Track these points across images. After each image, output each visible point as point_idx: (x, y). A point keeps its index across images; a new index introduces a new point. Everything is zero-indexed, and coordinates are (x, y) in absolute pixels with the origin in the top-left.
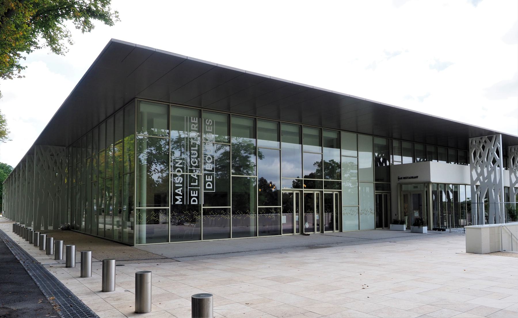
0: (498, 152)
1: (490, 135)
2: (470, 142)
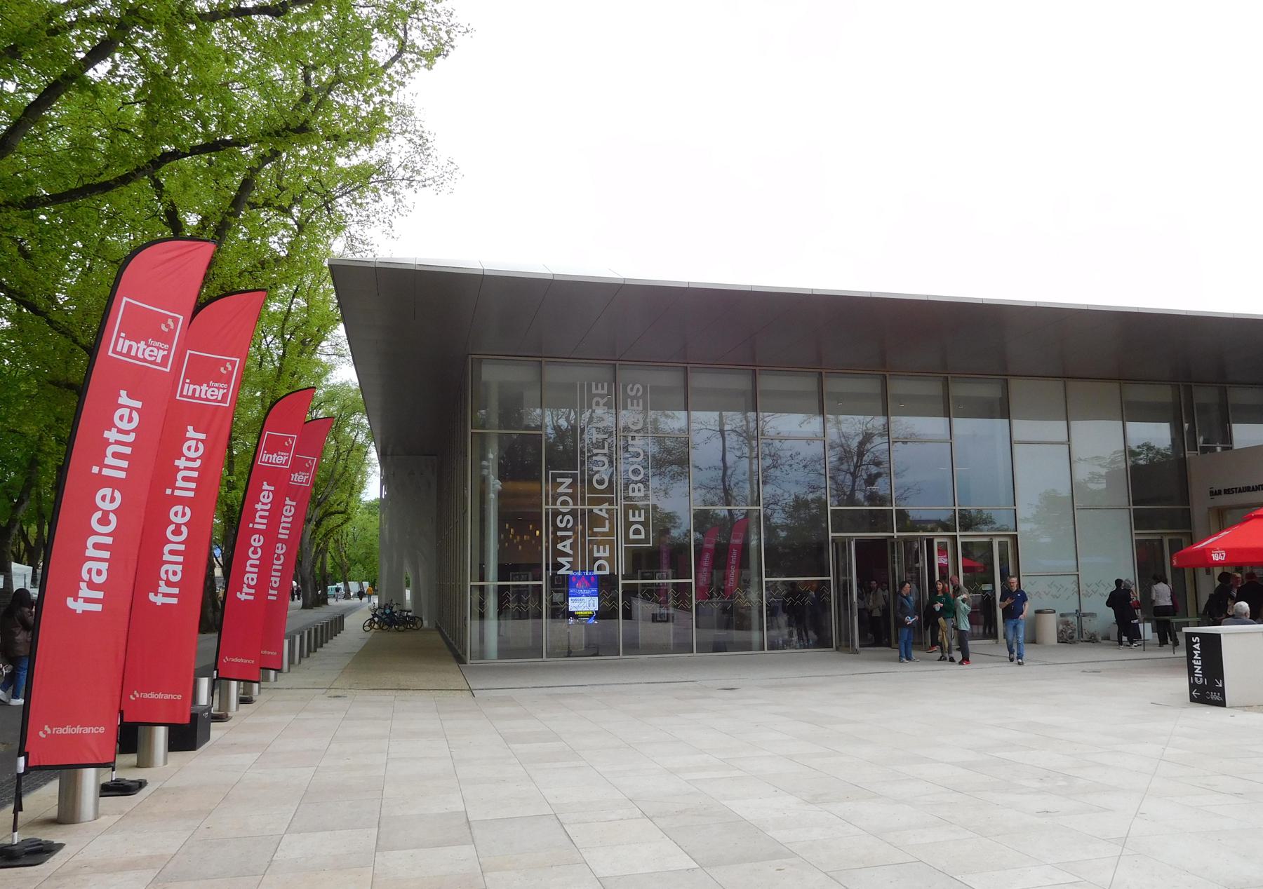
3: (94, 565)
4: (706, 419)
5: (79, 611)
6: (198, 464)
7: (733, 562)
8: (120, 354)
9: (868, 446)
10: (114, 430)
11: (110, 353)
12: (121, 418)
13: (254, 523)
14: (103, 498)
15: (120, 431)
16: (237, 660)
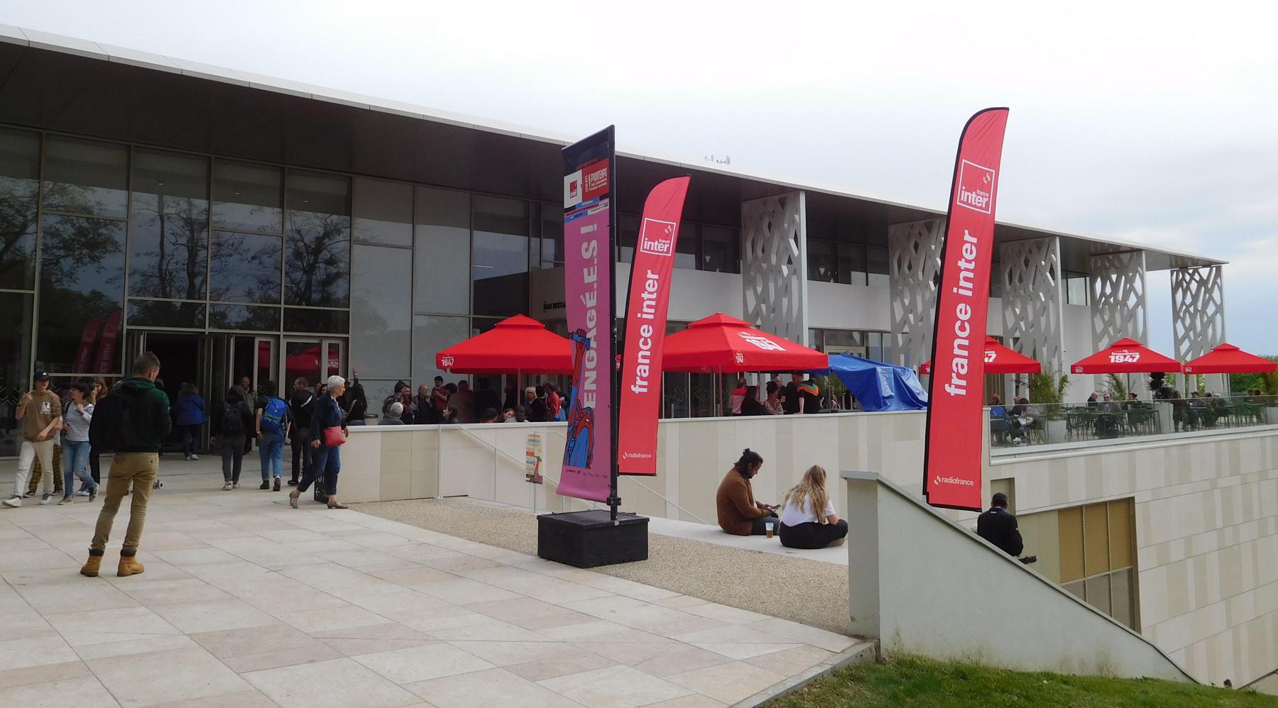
0: (1052, 272)
4: (146, 203)
6: (654, 296)
7: (83, 360)
9: (326, 241)
13: (642, 313)
16: (635, 455)
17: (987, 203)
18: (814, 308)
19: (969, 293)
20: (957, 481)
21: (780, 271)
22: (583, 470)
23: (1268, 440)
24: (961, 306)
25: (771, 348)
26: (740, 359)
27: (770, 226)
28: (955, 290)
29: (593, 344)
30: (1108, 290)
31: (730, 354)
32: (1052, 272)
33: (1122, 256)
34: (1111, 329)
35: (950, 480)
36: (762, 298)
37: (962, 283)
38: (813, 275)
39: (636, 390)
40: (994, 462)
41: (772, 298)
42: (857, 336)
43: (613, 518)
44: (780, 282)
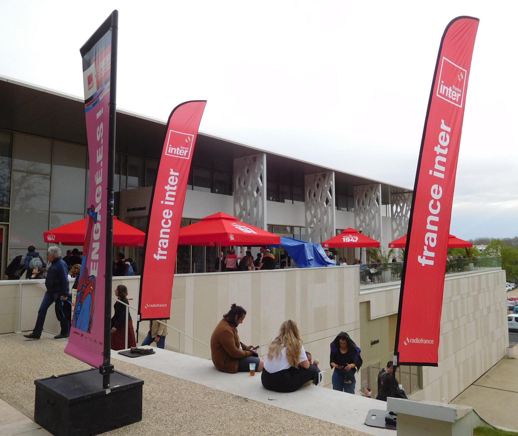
0: (378, 201)
1: (322, 173)
2: (355, 190)
3: (163, 241)
5: (158, 259)
6: (175, 188)
8: (170, 154)
10: (169, 185)
11: (166, 154)
12: (171, 180)
14: (166, 214)
15: (171, 186)
17: (460, 98)
18: (267, 214)
19: (442, 176)
20: (422, 341)
21: (253, 194)
22: (85, 334)
23: (470, 278)
24: (435, 187)
25: (249, 232)
26: (232, 238)
27: (248, 171)
28: (431, 172)
29: (99, 218)
30: (399, 210)
31: (226, 235)
32: (378, 201)
33: (405, 194)
34: (400, 227)
35: (416, 341)
36: (243, 208)
37: (437, 167)
38: (268, 199)
39: (157, 257)
40: (361, 293)
41: (249, 208)
42: (288, 229)
43: (105, 387)
44: (253, 200)
